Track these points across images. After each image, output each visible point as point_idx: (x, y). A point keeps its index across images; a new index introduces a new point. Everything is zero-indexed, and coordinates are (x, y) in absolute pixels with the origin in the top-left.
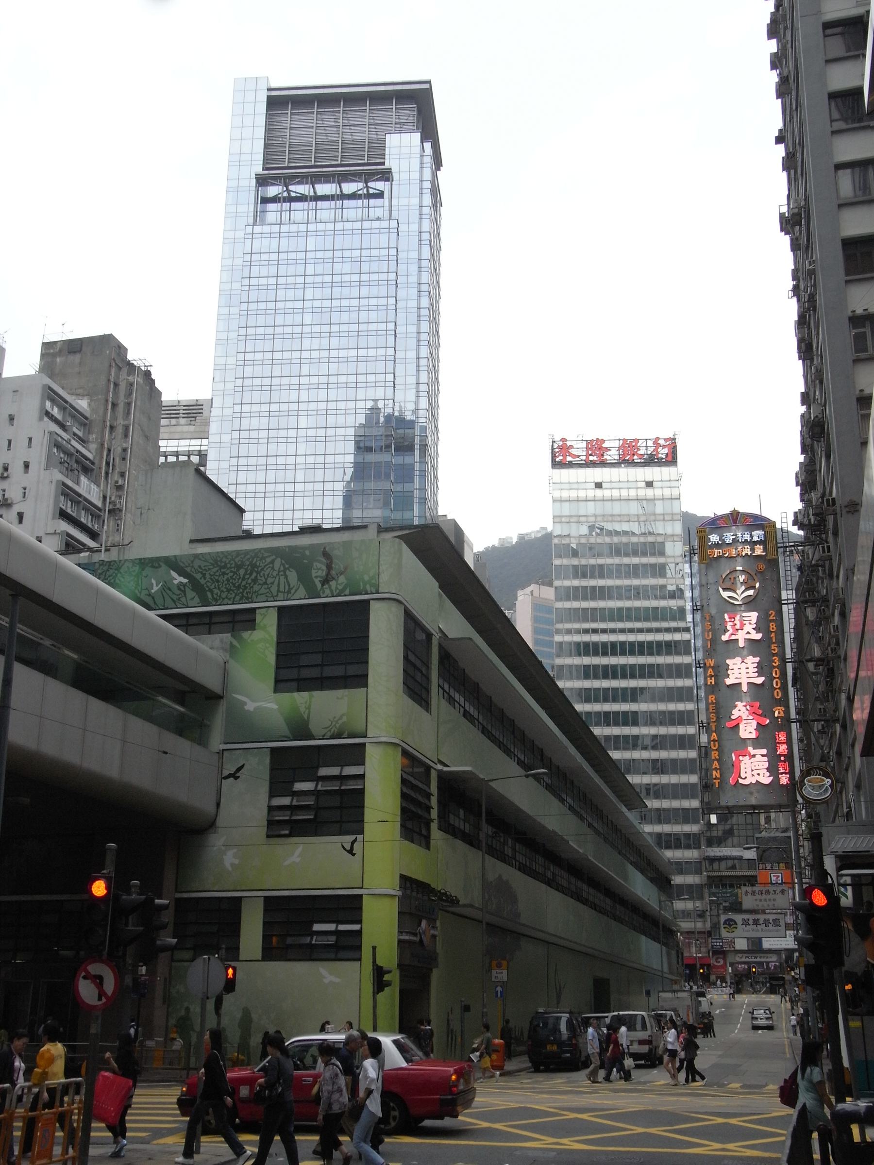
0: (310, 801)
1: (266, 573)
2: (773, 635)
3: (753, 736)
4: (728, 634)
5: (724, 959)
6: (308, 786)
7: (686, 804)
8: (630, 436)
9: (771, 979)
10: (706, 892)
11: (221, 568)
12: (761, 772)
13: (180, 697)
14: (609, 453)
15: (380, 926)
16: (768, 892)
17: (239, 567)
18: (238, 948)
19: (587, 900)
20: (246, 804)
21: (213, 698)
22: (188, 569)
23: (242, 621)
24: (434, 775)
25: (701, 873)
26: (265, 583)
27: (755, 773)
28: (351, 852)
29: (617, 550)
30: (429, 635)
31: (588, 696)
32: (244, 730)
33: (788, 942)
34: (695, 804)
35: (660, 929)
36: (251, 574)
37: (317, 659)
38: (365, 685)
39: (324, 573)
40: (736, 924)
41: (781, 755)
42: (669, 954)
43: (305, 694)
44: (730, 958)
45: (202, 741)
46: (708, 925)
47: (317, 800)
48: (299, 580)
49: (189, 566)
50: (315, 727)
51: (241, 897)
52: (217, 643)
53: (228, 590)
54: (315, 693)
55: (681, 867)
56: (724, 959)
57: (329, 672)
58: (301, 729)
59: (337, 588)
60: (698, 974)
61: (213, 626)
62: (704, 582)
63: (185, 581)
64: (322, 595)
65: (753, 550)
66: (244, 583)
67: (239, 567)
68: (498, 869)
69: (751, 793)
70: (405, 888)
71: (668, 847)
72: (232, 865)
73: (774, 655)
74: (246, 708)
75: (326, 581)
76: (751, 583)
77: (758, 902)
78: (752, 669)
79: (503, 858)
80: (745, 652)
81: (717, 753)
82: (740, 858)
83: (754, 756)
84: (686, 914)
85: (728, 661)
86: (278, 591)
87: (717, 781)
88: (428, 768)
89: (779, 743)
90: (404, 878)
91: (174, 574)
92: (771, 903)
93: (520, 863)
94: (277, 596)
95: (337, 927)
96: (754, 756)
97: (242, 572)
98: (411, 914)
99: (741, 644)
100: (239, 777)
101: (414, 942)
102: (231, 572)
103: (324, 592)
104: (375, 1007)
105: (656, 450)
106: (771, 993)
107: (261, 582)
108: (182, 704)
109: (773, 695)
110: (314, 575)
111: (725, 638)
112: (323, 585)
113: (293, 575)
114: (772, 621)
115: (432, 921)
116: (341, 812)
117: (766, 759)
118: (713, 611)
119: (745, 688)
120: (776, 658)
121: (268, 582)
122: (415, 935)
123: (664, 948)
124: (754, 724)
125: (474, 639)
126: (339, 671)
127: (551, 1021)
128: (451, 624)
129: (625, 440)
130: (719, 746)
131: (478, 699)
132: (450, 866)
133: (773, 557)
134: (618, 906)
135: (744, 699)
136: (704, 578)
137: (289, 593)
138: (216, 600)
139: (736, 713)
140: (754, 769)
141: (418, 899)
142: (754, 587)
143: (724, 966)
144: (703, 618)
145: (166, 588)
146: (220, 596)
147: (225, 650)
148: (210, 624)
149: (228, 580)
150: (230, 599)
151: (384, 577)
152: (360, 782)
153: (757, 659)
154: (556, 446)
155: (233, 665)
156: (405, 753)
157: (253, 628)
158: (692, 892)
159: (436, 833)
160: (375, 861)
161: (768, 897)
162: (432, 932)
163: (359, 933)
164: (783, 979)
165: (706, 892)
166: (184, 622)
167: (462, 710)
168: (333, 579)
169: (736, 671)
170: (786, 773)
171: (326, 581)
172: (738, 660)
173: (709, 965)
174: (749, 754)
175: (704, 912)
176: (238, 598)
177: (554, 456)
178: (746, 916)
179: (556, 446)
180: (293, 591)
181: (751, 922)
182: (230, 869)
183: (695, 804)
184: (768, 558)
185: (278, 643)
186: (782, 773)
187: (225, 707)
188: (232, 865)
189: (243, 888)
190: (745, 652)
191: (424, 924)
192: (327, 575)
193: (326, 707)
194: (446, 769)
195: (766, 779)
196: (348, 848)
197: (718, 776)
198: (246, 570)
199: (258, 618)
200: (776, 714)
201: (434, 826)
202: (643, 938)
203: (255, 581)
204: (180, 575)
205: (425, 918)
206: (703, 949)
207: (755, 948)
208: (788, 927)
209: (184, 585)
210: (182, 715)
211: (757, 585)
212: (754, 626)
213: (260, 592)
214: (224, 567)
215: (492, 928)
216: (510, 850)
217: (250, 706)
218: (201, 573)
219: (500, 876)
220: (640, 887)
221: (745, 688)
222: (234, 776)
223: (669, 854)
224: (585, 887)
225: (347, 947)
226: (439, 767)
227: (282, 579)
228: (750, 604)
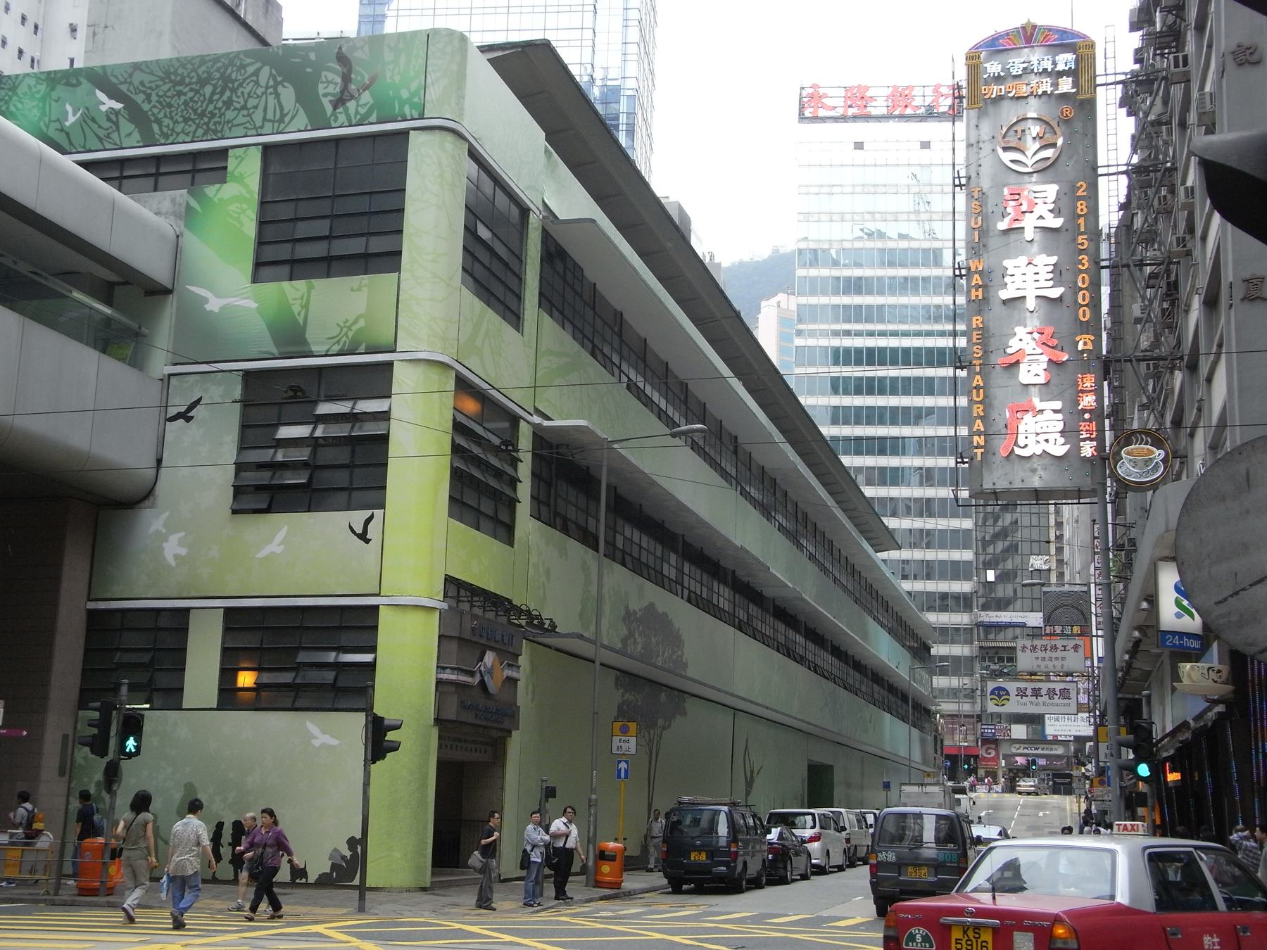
0: (302, 454)
1: (246, 91)
2: (1081, 221)
3: (1042, 380)
4: (1007, 220)
5: (997, 749)
6: (301, 431)
7: (956, 555)
8: (902, 82)
9: (1055, 775)
10: (977, 665)
11: (176, 83)
12: (1051, 437)
13: (106, 293)
14: (874, 104)
15: (407, 662)
16: (1054, 648)
17: (203, 82)
18: (181, 690)
19: (801, 657)
20: (202, 461)
21: (158, 292)
22: (124, 88)
23: (206, 167)
24: (525, 430)
25: (972, 643)
26: (244, 107)
27: (1041, 438)
28: (363, 537)
29: (889, 258)
30: (525, 211)
31: (838, 415)
32: (203, 342)
33: (1082, 726)
34: (968, 555)
35: (917, 711)
36: (222, 93)
37: (322, 228)
38: (397, 268)
39: (338, 89)
40: (1008, 694)
41: (1084, 411)
42: (923, 741)
43: (301, 285)
44: (1004, 749)
45: (137, 362)
46: (978, 708)
47: (314, 454)
48: (297, 101)
49: (125, 82)
50: (317, 338)
51: (188, 610)
52: (166, 205)
53: (186, 120)
54: (315, 282)
55: (947, 634)
56: (997, 749)
57: (341, 247)
58: (291, 336)
59: (357, 112)
60: (960, 767)
61: (162, 179)
62: (973, 140)
63: (118, 106)
64: (333, 125)
65: (1055, 85)
66: (211, 107)
67: (203, 82)
68: (646, 594)
69: (1034, 471)
70: (458, 599)
71: (931, 609)
72: (176, 557)
73: (1081, 252)
74: (208, 307)
75: (339, 102)
76: (1049, 138)
77: (1039, 662)
78: (1045, 274)
79: (659, 580)
80: (1035, 248)
81: (982, 407)
82: (1023, 626)
83: (1042, 411)
84: (954, 693)
85: (1006, 263)
86: (265, 119)
87: (979, 451)
88: (515, 420)
89: (1083, 392)
90: (449, 580)
91: (101, 96)
92: (1058, 664)
93: (690, 591)
94: (262, 127)
95: (337, 656)
96: (1042, 411)
97: (208, 90)
98: (460, 639)
99: (1029, 234)
100: (192, 418)
101: (465, 686)
102: (191, 90)
103: (336, 120)
104: (366, 784)
105: (936, 100)
106: (1055, 793)
107: (238, 106)
108: (108, 302)
109: (1076, 283)
110: (321, 91)
111: (1002, 225)
112: (335, 108)
113: (288, 94)
114: (1080, 198)
115: (510, 657)
116: (348, 472)
117: (1060, 416)
118: (985, 184)
119: (1031, 304)
120: (1085, 258)
121: (249, 106)
122: (472, 674)
123: (915, 732)
124: (1045, 358)
125: (599, 222)
126: (355, 246)
127: (705, 819)
128: (562, 197)
129: (895, 88)
130: (985, 396)
131: (686, 403)
132: (538, 566)
133: (1088, 96)
134: (851, 672)
135: (1028, 322)
136: (973, 132)
137: (281, 121)
138: (166, 136)
139: (1014, 345)
140: (1041, 433)
141: (476, 619)
142: (1054, 145)
143: (996, 759)
144: (970, 196)
145: (89, 118)
146: (173, 130)
147: (177, 216)
148: (157, 175)
149: (186, 103)
150: (187, 134)
151: (433, 94)
152: (383, 425)
153: (1054, 259)
154: (804, 93)
155: (192, 242)
156: (463, 385)
157: (223, 181)
158: (955, 666)
159: (526, 523)
160: (402, 553)
161: (1054, 655)
162: (508, 672)
163: (372, 666)
164: (1070, 776)
165: (977, 665)
166: (116, 174)
167: (625, 379)
168: (352, 97)
169: (1018, 278)
170: (1091, 439)
171: (339, 102)
172: (1022, 260)
173: (976, 757)
174: (1033, 408)
175: (973, 691)
176: (200, 132)
177: (802, 108)
178: (1022, 685)
179: (804, 93)
180: (287, 119)
181: (1029, 692)
182: (173, 564)
183: (968, 555)
184: (1079, 97)
185: (263, 203)
186: (1084, 440)
187: (174, 310)
188: (176, 557)
189: (193, 594)
190: (1035, 248)
191: (489, 658)
192: (342, 92)
193: (334, 309)
194: (546, 423)
195: (1059, 448)
196: (359, 531)
197: (982, 443)
198: (215, 87)
199: (231, 163)
200: (1080, 347)
201: (524, 509)
202: (887, 716)
203: (228, 104)
204: (111, 97)
205: (491, 648)
206: (970, 738)
207: (1036, 737)
208: (1080, 708)
209: (117, 113)
210: (108, 320)
211: (1060, 142)
212: (1051, 207)
213: (235, 122)
214: (182, 82)
215: (627, 678)
216: (673, 571)
217: (214, 305)
218: (144, 93)
219: (652, 605)
220: (884, 650)
221: (1031, 304)
222: (185, 416)
223: (932, 618)
224: (800, 639)
225: (351, 689)
226: (536, 419)
227: (272, 100)
228: (1046, 170)
